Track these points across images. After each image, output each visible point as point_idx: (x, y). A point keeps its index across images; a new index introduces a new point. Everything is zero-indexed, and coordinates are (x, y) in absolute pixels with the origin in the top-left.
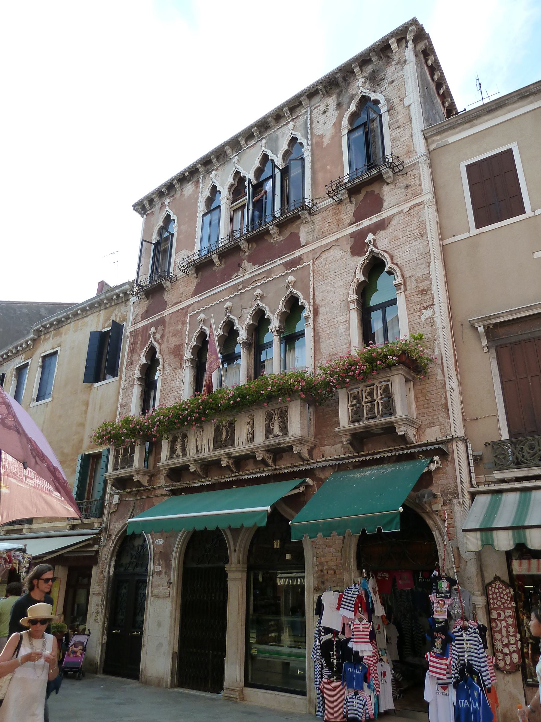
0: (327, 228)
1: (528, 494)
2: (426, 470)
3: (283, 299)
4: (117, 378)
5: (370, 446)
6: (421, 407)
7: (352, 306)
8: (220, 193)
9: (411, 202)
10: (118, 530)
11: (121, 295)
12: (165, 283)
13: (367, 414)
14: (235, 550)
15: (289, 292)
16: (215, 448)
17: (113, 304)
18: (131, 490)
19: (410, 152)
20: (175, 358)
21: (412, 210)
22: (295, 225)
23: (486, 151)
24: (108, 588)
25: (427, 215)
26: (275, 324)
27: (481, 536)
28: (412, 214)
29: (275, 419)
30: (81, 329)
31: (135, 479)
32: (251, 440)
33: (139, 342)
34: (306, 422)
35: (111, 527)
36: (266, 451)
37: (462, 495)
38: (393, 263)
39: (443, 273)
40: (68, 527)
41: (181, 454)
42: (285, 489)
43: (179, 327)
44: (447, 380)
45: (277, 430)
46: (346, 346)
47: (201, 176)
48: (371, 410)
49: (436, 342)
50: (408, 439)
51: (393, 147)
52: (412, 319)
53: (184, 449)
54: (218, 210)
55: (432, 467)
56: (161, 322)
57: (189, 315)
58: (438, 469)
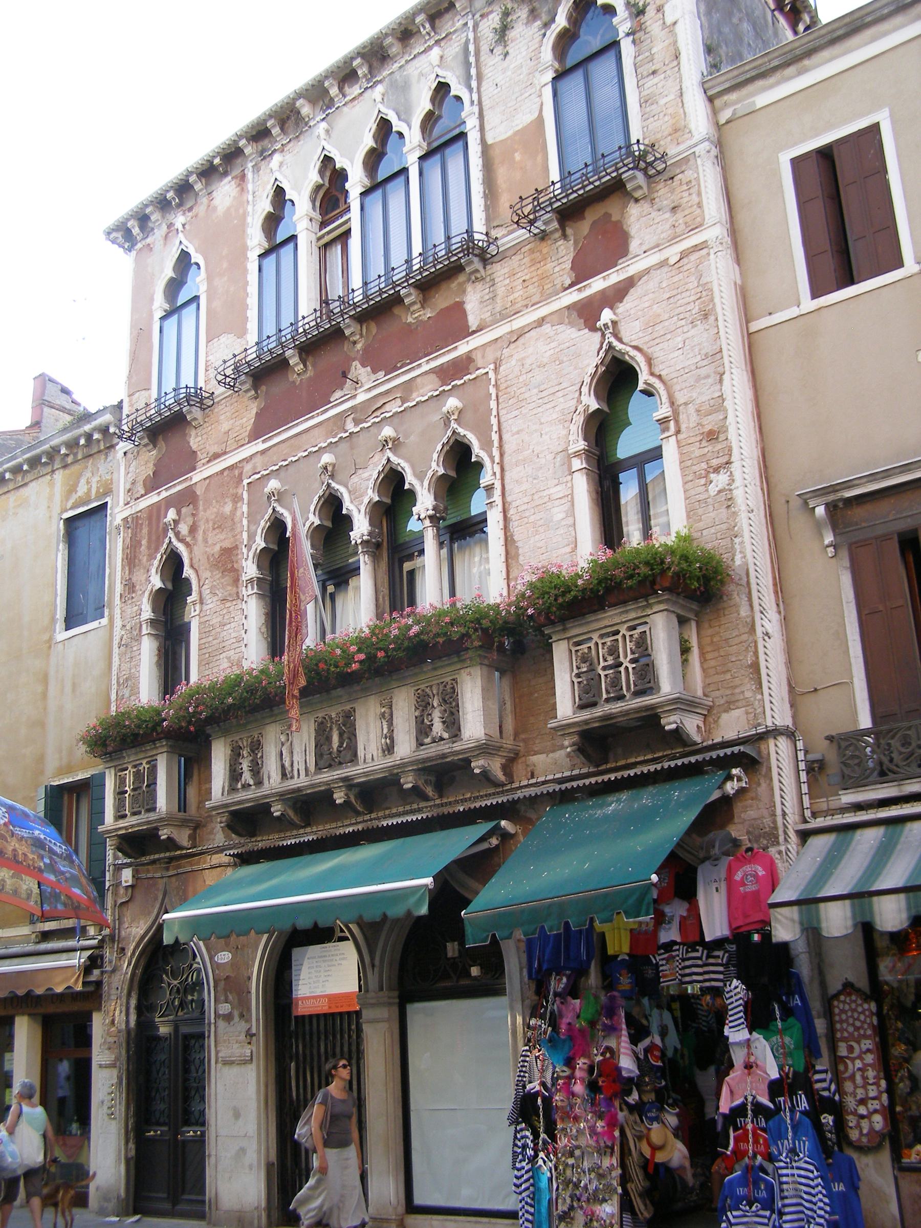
0: (521, 293)
1: (899, 828)
2: (716, 795)
3: (439, 447)
4: (104, 621)
5: (620, 751)
6: (712, 671)
7: (577, 464)
8: (293, 204)
9: (513, 322)
10: (137, 939)
11: (96, 436)
12: (190, 412)
13: (608, 692)
14: (373, 966)
15: (449, 433)
16: (319, 768)
17: (80, 457)
18: (157, 856)
19: (679, 130)
20: (223, 576)
21: (685, 260)
22: (454, 285)
23: (830, 127)
24: (128, 1051)
25: (714, 272)
26: (425, 502)
27: (801, 913)
28: (685, 268)
29: (433, 706)
30: (16, 514)
31: (164, 834)
32: (389, 749)
33: (144, 542)
34: (495, 708)
35: (123, 933)
36: (419, 770)
37: (785, 838)
38: (652, 374)
39: (749, 394)
40: (34, 936)
41: (252, 782)
42: (457, 843)
43: (228, 509)
44: (758, 616)
45: (438, 728)
46: (568, 549)
47: (250, 165)
48: (615, 683)
49: (737, 540)
50: (685, 737)
51: (645, 117)
52: (693, 492)
53: (256, 770)
54: (291, 246)
55: (731, 787)
56: (188, 498)
57: (246, 482)
58: (741, 791)
